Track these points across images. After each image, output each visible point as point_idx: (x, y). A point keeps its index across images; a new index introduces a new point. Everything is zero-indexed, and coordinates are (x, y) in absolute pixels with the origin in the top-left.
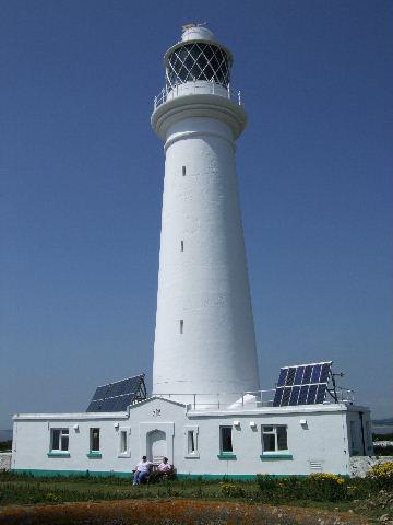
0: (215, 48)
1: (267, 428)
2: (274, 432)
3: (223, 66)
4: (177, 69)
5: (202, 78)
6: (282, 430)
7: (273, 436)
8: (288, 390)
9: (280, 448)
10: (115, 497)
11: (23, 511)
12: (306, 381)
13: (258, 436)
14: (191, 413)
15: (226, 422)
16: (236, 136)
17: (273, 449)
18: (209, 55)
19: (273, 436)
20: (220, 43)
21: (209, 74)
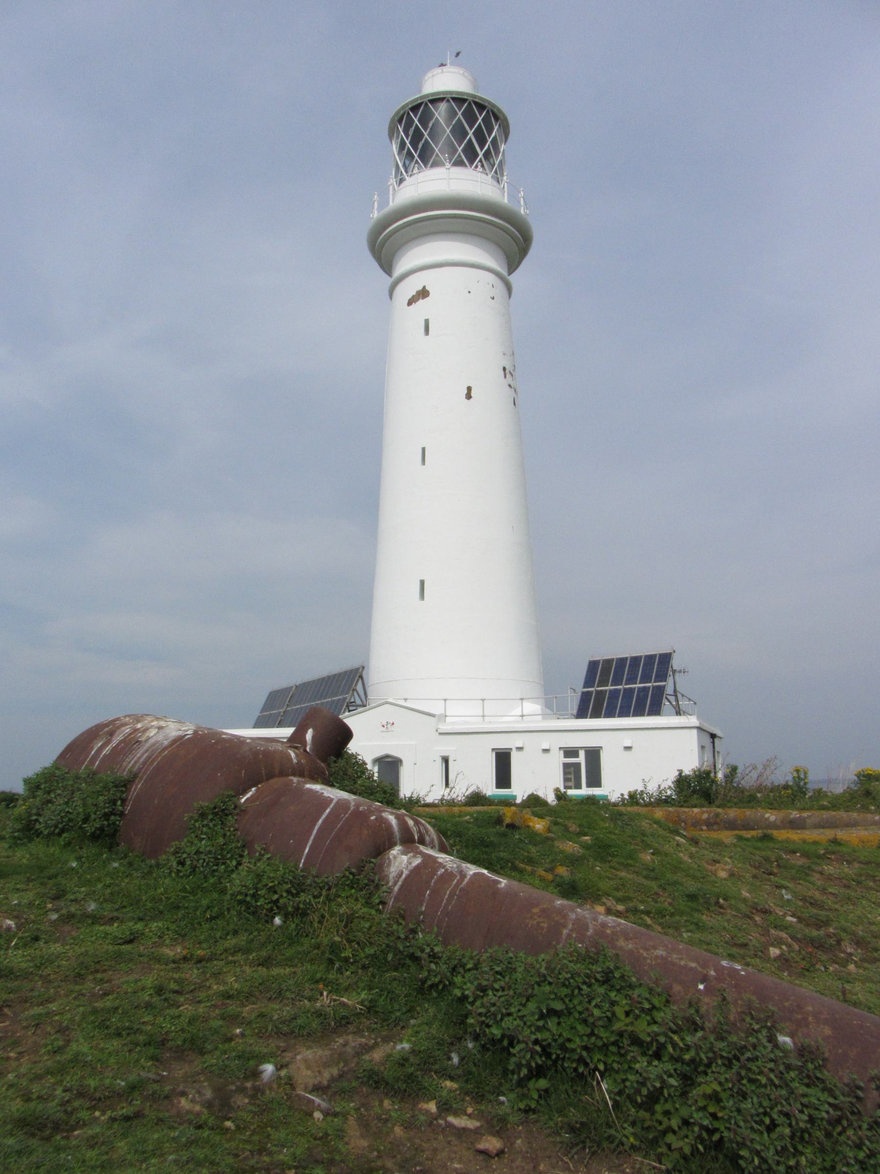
0: (481, 107)
1: (570, 752)
2: (582, 759)
3: (494, 142)
4: (414, 144)
5: (459, 163)
6: (594, 755)
7: (579, 764)
8: (601, 694)
9: (590, 785)
10: (140, 758)
11: (487, 813)
12: (632, 680)
13: (558, 760)
14: (444, 728)
15: (503, 743)
16: (513, 264)
17: (578, 786)
18: (471, 120)
19: (579, 764)
20: (486, 95)
21: (471, 155)
